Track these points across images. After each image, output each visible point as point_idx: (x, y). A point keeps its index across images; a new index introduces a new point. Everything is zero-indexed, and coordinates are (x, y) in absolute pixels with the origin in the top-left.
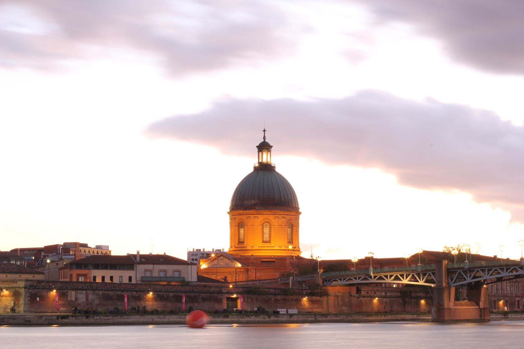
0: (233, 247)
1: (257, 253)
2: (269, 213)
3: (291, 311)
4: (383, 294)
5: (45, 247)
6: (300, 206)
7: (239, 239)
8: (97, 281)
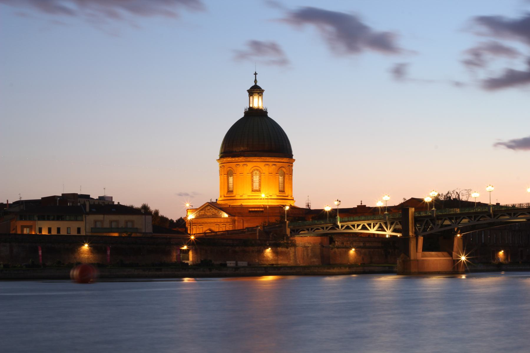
0: (223, 197)
1: (246, 202)
2: (259, 160)
3: (241, 264)
4: (362, 244)
5: (44, 199)
6: (293, 154)
7: (228, 187)
8: (43, 233)
